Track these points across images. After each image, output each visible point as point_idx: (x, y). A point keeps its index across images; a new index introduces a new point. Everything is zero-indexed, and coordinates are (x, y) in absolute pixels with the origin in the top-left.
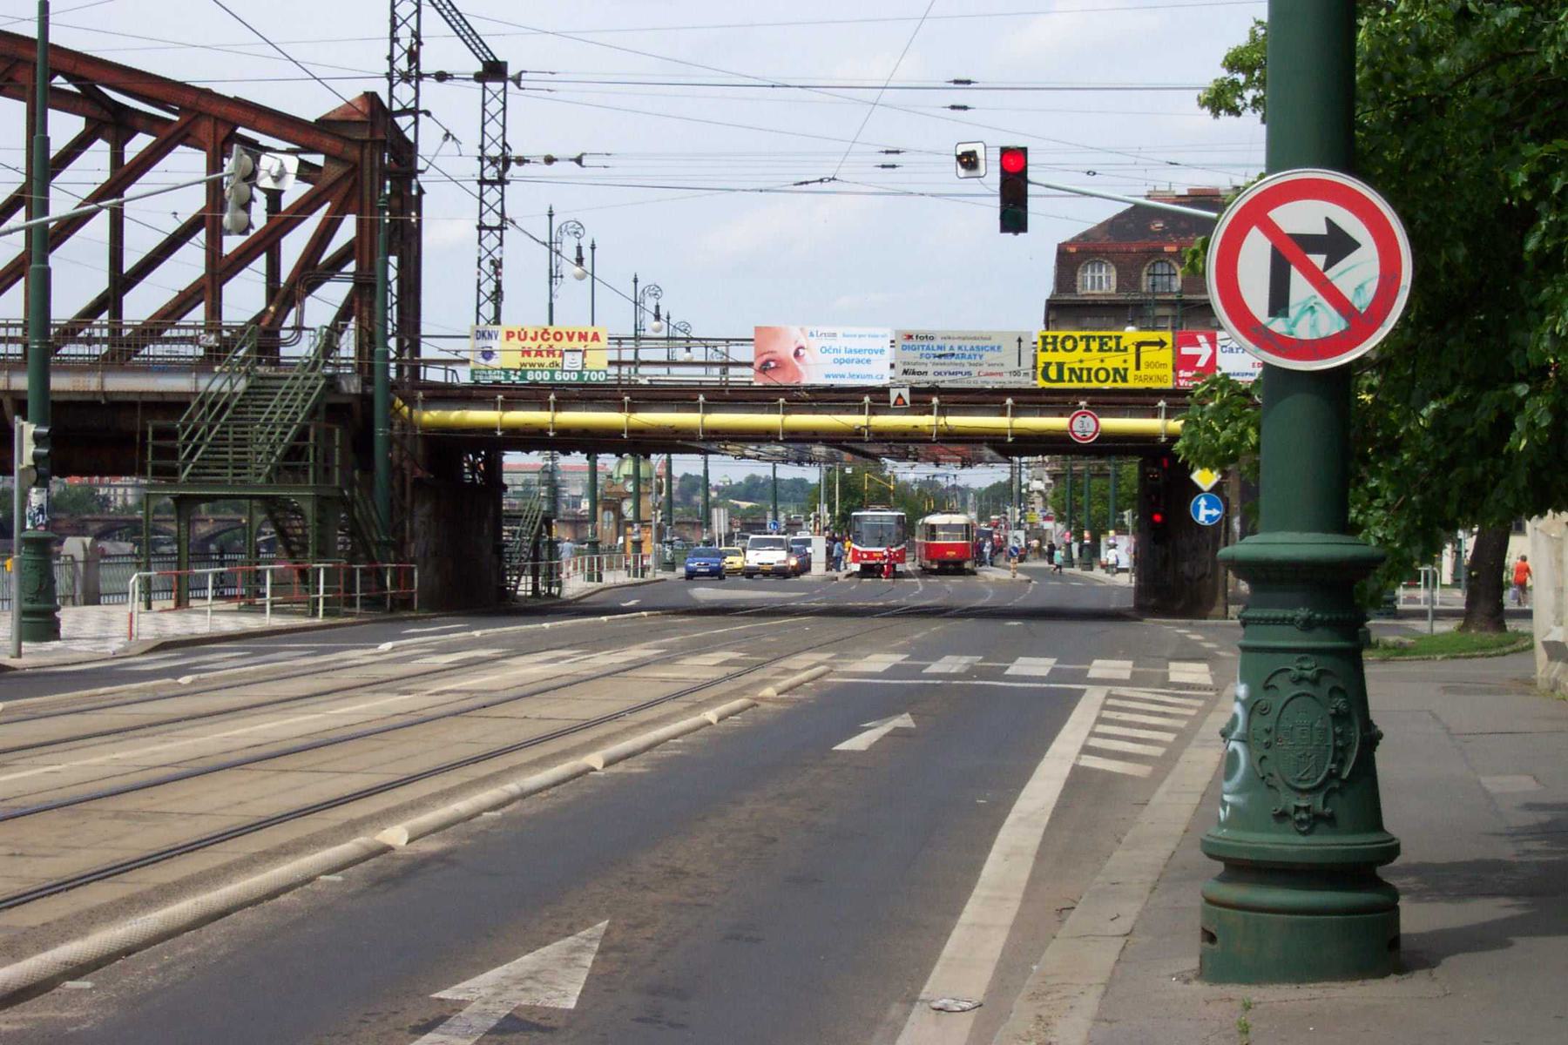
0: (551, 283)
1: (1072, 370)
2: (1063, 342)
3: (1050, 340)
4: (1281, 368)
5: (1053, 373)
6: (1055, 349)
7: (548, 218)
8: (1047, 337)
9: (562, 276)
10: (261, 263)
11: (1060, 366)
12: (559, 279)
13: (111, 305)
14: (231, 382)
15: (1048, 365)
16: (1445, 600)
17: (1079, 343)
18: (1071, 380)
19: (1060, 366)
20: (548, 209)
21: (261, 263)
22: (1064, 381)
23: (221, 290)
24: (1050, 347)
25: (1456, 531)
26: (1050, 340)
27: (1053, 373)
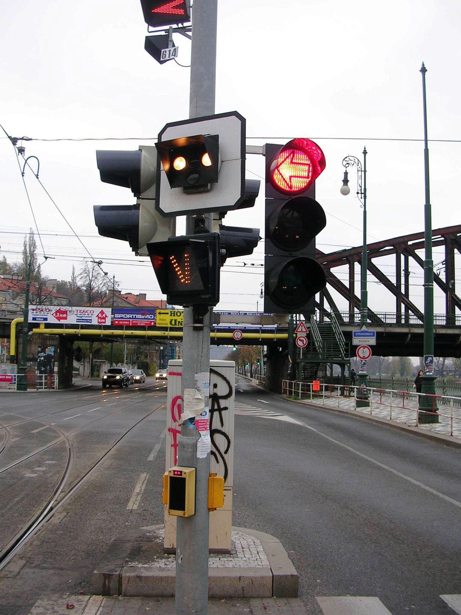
0: (365, 189)
1: (179, 322)
2: (177, 313)
3: (173, 313)
4: (10, 333)
5: (173, 322)
6: (174, 316)
7: (420, 74)
8: (172, 312)
9: (358, 193)
10: (422, 310)
11: (176, 320)
12: (360, 192)
13: (446, 285)
14: (417, 259)
15: (172, 320)
16: (14, 384)
17: (182, 314)
18: (178, 325)
19: (176, 320)
20: (422, 63)
21: (422, 310)
22: (176, 325)
23: (348, 300)
24: (173, 315)
25: (58, 362)
26: (173, 313)
27: (173, 322)
